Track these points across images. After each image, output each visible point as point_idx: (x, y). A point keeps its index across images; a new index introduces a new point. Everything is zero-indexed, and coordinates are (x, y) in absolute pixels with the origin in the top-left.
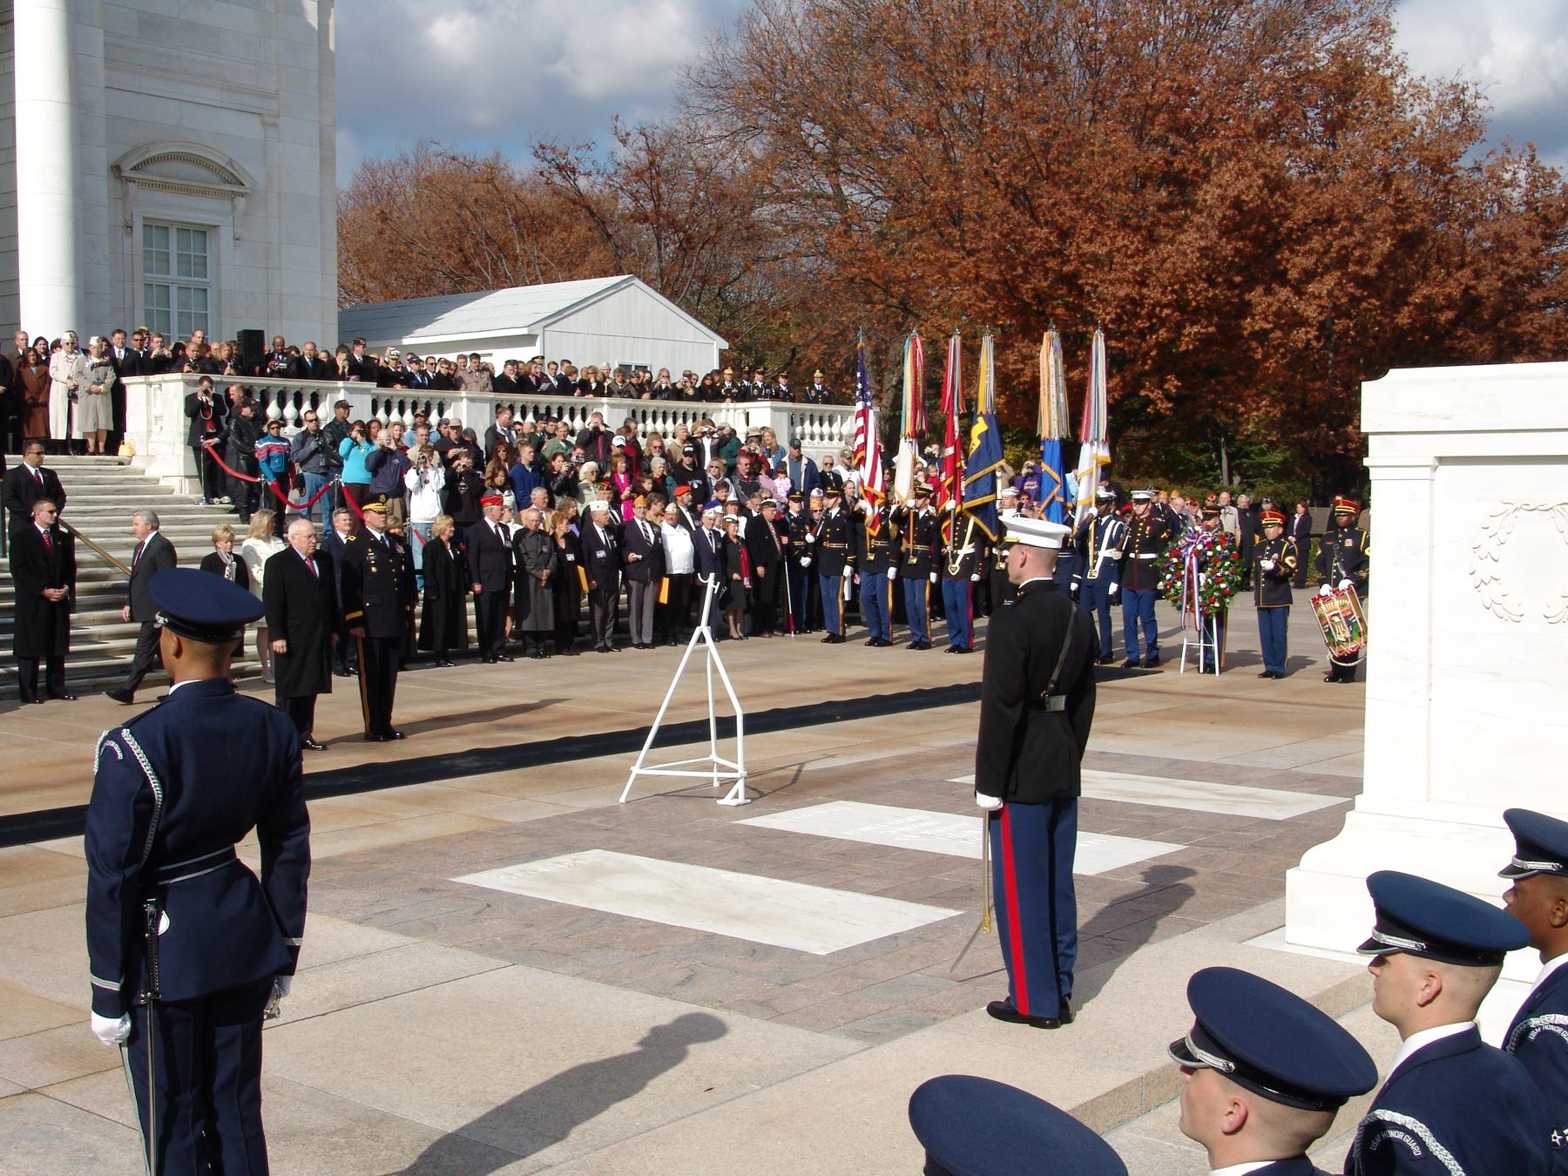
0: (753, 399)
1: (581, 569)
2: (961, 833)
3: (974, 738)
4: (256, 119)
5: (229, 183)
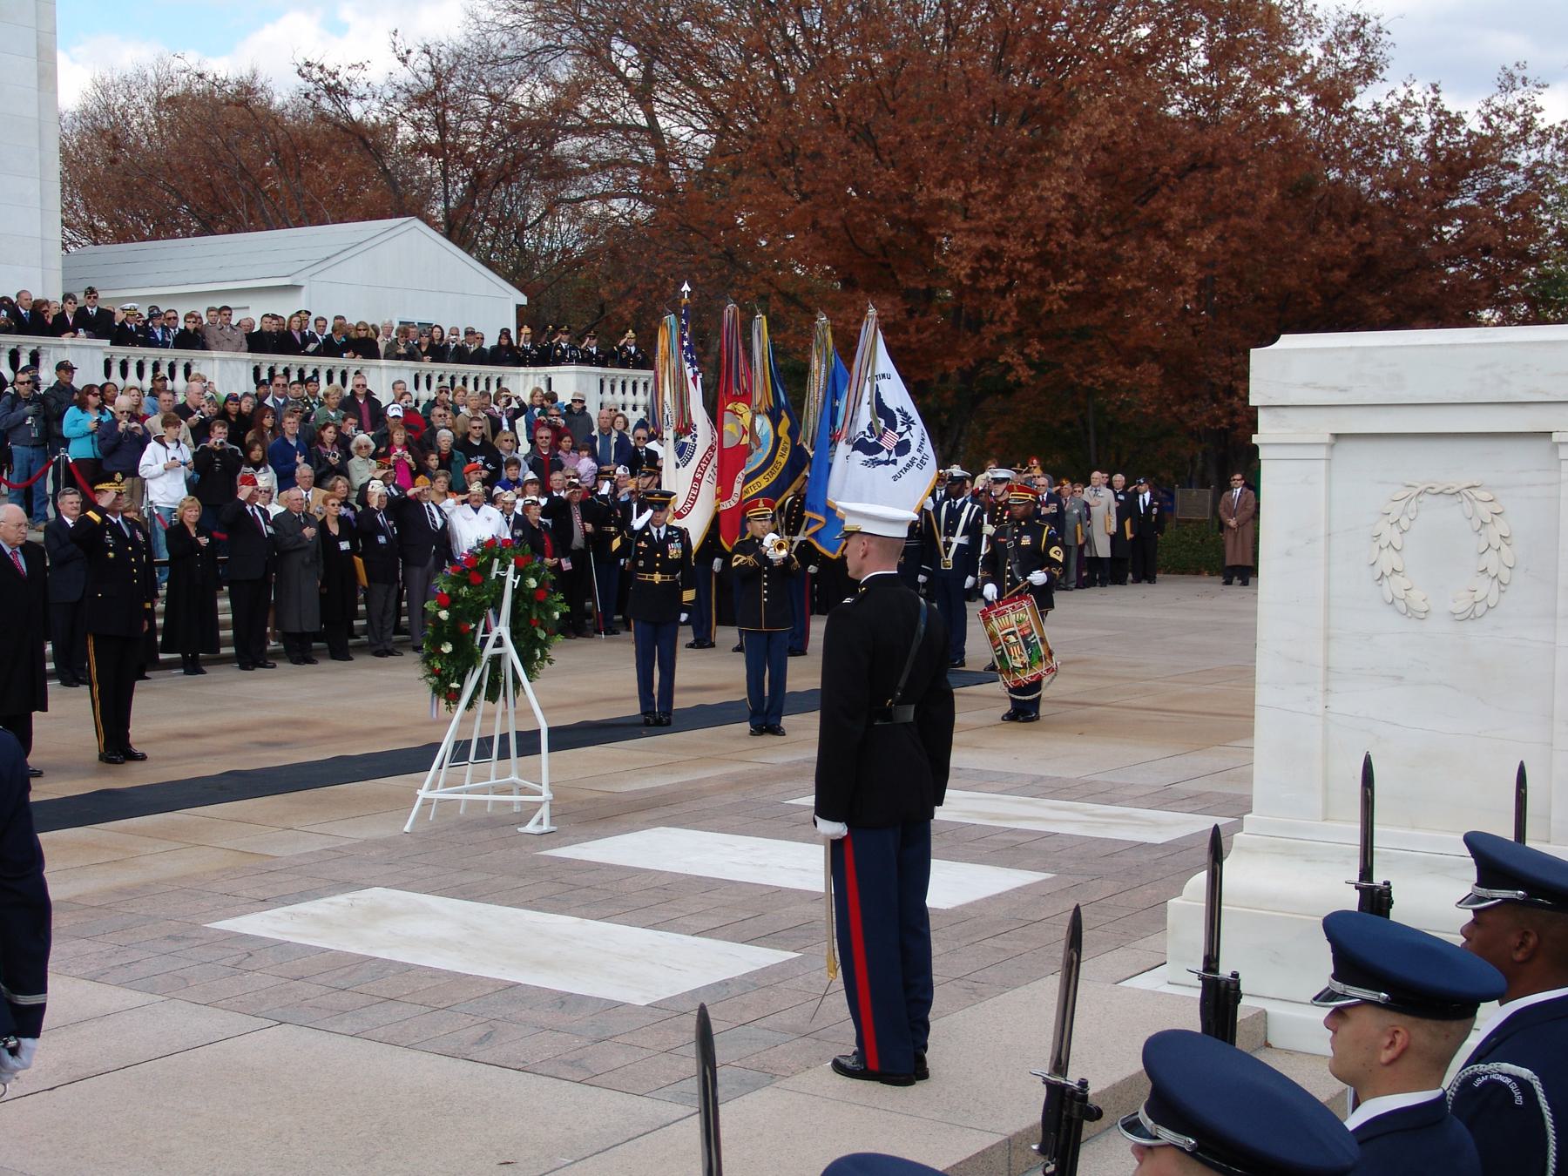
0: (558, 361)
1: (359, 561)
2: (800, 864)
3: (814, 753)
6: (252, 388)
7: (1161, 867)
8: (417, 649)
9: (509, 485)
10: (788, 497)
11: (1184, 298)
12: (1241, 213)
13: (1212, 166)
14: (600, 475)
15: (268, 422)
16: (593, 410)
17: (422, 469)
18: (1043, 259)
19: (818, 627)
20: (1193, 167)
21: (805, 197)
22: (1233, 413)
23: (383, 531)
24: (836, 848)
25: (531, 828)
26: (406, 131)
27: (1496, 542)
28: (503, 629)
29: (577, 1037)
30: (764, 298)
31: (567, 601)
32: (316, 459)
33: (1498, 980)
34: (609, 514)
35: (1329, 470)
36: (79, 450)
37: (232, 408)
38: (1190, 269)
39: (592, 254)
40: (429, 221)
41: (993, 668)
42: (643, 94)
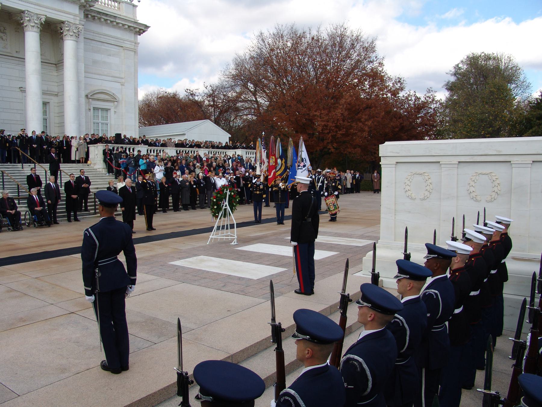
0: (237, 148)
1: (197, 189)
2: (287, 251)
3: (290, 228)
4: (120, 84)
5: (113, 99)
6: (176, 155)
7: (363, 250)
8: (209, 207)
9: (227, 174)
10: (285, 175)
11: (365, 134)
12: (377, 117)
13: (370, 108)
14: (246, 172)
15: (179, 161)
16: (244, 158)
17: (210, 171)
18: (336, 127)
19: (291, 203)
20: (367, 108)
21: (287, 114)
22: (376, 158)
23: (202, 183)
24: (295, 247)
25: (233, 243)
26: (206, 102)
27: (429, 184)
28: (227, 203)
29: (243, 286)
30: (279, 135)
31: (240, 197)
32: (189, 169)
33: (430, 272)
34: (248, 179)
35: (395, 170)
36: (143, 167)
37: (172, 159)
38: (366, 129)
39: (244, 126)
40: (211, 120)
41: (327, 210)
42: (254, 94)
